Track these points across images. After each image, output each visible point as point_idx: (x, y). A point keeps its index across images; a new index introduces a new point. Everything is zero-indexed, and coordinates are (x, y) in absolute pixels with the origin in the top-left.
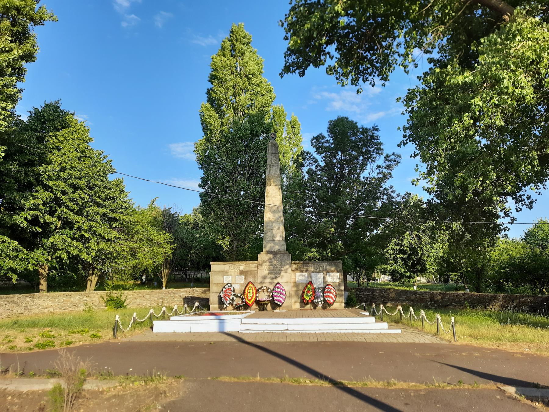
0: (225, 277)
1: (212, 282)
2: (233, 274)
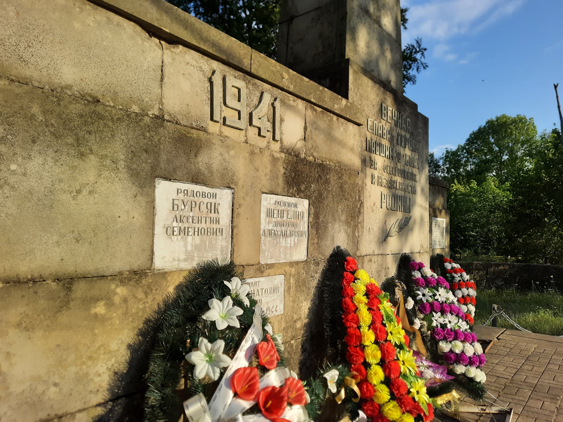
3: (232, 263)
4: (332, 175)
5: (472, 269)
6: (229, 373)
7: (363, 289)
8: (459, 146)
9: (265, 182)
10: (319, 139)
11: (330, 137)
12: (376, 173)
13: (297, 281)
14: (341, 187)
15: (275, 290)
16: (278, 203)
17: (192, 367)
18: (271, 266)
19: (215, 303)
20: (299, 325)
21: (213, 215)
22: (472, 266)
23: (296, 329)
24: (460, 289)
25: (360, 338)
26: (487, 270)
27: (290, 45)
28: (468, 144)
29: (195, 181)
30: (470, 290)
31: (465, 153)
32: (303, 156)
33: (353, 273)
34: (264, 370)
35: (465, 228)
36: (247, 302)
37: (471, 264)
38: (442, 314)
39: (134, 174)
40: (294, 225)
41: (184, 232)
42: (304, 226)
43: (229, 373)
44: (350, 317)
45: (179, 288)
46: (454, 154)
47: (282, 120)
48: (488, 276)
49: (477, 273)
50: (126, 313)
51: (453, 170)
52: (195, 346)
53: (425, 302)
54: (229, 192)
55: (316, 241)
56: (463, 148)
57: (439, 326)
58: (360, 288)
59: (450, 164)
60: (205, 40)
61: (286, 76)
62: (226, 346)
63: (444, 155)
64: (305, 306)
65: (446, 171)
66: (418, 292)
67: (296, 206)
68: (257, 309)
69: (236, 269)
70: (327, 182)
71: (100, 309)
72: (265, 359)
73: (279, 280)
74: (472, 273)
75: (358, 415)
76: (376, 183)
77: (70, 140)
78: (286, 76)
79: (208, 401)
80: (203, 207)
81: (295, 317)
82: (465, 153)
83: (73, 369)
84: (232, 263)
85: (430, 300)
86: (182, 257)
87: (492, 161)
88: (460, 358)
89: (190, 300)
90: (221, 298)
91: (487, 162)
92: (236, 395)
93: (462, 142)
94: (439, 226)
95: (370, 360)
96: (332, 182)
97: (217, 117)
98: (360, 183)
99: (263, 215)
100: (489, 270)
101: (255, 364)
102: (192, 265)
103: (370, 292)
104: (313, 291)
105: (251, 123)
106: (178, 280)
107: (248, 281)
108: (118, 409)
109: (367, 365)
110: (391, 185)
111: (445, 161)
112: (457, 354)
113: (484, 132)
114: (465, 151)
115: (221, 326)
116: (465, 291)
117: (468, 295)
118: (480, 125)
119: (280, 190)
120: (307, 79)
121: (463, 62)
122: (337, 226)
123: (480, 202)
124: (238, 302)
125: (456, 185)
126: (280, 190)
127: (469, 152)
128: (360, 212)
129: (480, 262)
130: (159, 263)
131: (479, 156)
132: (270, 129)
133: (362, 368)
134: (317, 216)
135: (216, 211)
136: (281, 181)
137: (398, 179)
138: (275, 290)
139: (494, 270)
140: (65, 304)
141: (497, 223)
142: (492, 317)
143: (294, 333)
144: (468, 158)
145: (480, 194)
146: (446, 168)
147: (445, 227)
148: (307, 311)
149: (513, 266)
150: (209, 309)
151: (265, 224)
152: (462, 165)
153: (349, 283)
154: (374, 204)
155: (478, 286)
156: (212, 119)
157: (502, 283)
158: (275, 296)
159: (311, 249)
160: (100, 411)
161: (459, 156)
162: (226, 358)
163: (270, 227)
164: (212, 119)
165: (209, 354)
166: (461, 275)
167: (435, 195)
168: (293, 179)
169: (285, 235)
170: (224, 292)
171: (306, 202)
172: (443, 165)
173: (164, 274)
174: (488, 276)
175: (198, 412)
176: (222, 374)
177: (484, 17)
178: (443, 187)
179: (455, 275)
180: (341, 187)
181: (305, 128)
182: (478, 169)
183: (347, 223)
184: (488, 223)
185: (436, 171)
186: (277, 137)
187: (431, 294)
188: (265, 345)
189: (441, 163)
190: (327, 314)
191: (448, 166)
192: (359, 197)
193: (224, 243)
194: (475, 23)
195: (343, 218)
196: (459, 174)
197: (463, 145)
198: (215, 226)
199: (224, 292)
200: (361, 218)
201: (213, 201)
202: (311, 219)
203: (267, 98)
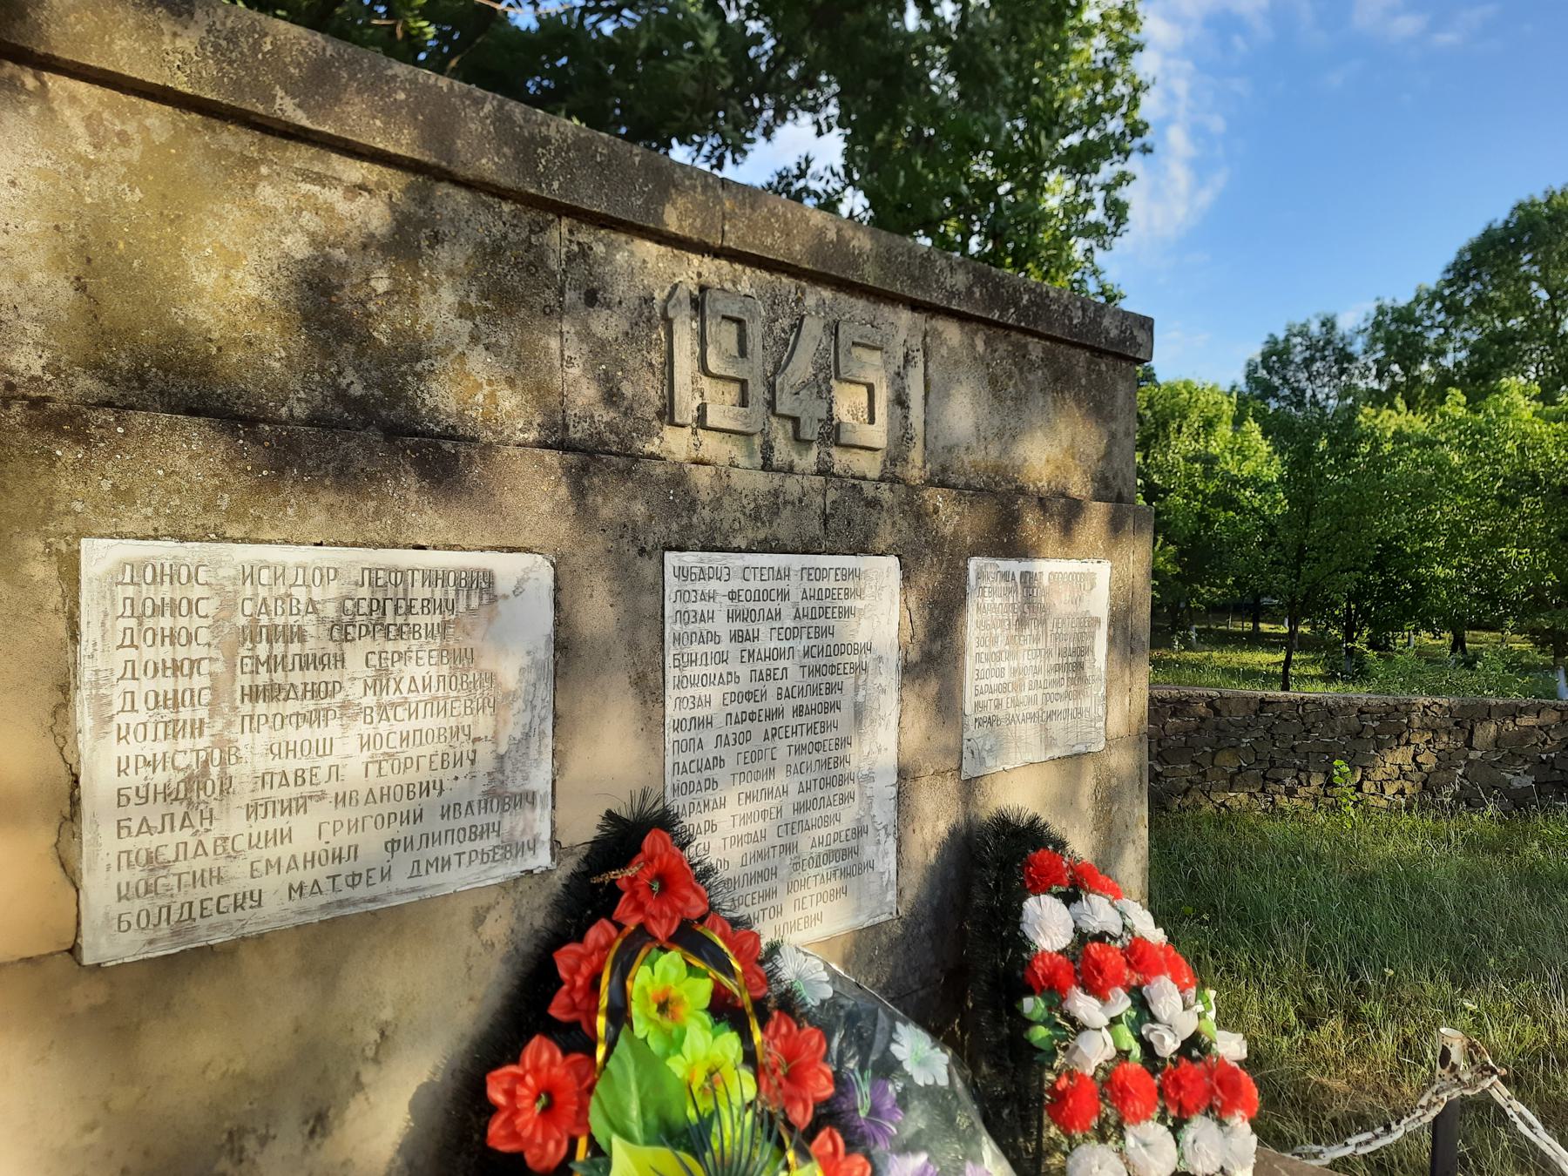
26: (1471, 733)
28: (1450, 283)
31: (1439, 312)
35: (1418, 555)
37: (1402, 708)
46: (1404, 316)
48: (1472, 755)
49: (1428, 742)
51: (1395, 368)
56: (1436, 296)
59: (1387, 349)
63: (1371, 321)
65: (1374, 372)
74: (1408, 743)
82: (1439, 312)
87: (1525, 337)
93: (1432, 275)
100: (1478, 732)
113: (1503, 241)
114: (1438, 305)
121: (1446, 38)
123: (1473, 465)
125: (1399, 413)
127: (1453, 309)
131: (1482, 323)
139: (1499, 730)
141: (1526, 540)
142: (1431, 1104)
144: (1446, 329)
145: (1475, 440)
146: (1376, 361)
152: (1427, 350)
157: (1529, 781)
161: (1418, 322)
167: (1019, 399)
172: (1366, 352)
174: (1472, 755)
178: (1097, 352)
179: (1084, 1005)
182: (1479, 361)
184: (1495, 540)
189: (1358, 347)
191: (1380, 355)
196: (1417, 380)
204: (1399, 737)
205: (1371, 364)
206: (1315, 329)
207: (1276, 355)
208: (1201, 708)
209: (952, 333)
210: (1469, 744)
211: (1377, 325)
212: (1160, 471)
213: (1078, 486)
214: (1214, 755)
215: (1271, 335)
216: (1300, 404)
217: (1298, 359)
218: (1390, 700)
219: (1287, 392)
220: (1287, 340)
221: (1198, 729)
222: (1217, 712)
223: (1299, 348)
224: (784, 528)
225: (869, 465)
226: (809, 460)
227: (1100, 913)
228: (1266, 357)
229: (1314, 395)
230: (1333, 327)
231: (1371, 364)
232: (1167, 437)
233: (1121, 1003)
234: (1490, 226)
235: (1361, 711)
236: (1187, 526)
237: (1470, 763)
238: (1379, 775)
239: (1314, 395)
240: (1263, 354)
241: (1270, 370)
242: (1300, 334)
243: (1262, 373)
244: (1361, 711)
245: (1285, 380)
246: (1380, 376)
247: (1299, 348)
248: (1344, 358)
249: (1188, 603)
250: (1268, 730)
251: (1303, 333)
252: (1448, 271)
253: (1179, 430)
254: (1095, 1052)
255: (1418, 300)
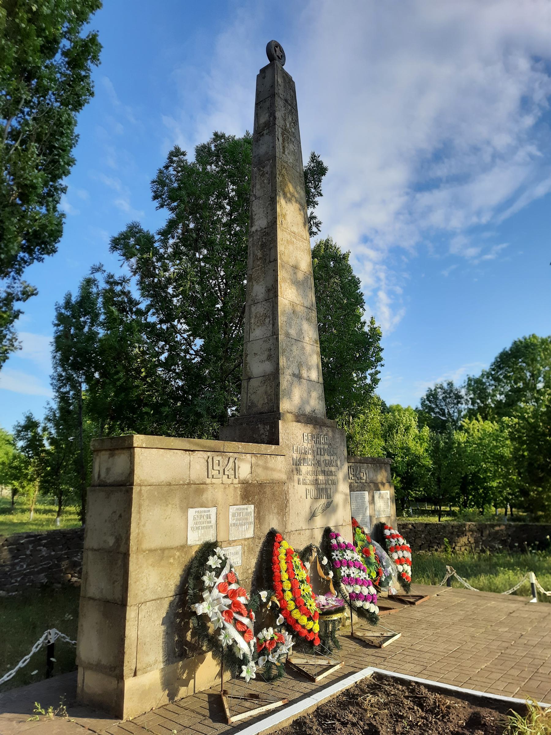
0: (192, 512)
1: (139, 542)
2: (219, 495)
3: (217, 541)
4: (267, 488)
5: (465, 530)
6: (217, 584)
7: (284, 551)
8: (483, 371)
9: (231, 500)
10: (259, 471)
11: (266, 468)
12: (301, 478)
13: (249, 548)
14: (273, 494)
15: (237, 553)
16: (237, 509)
17: (204, 582)
18: (235, 541)
19: (211, 558)
20: (250, 571)
21: (208, 520)
22: (465, 527)
23: (248, 574)
24: (396, 552)
25: (280, 577)
27: (249, 395)
29: (202, 507)
30: (405, 552)
32: (250, 482)
33: (279, 543)
34: (230, 584)
35: (484, 478)
36: (223, 558)
38: (348, 568)
39: (181, 508)
40: (247, 519)
41: (198, 528)
42: (251, 519)
43: (217, 584)
44: (275, 566)
45: (196, 552)
46: (478, 381)
47: (239, 467)
48: (484, 538)
50: (179, 562)
51: (478, 401)
52: (204, 574)
53: (337, 560)
54: (215, 508)
55: (259, 526)
56: (488, 375)
57: (346, 576)
58: (282, 552)
60: (205, 447)
61: (240, 447)
62: (216, 574)
63: (466, 383)
64: (253, 562)
65: (470, 402)
66: (333, 553)
67: (247, 509)
68: (228, 561)
69: (219, 544)
70: (265, 493)
71: (172, 560)
72: (230, 579)
73: (239, 548)
74: (466, 535)
75: (279, 616)
76: (302, 484)
77: (164, 501)
78: (240, 447)
79: (210, 593)
80: (205, 517)
81: (248, 567)
83: (164, 582)
84: (217, 541)
85: (341, 558)
86: (197, 539)
88: (359, 596)
89: (201, 557)
90: (213, 556)
91: (519, 390)
92: (220, 592)
94: (383, 498)
95: (285, 588)
96: (268, 493)
97: (210, 476)
98: (286, 489)
99: (230, 516)
101: (227, 580)
102: (201, 542)
103: (288, 553)
104: (257, 553)
105: (224, 474)
106: (196, 549)
107: (224, 549)
108: (177, 599)
109: (284, 591)
110: (316, 482)
111: (469, 390)
112: (357, 594)
114: (491, 378)
115: (214, 567)
116: (400, 553)
117: (403, 557)
118: (504, 347)
119: (238, 503)
120: (251, 444)
121: (488, 257)
122: (271, 516)
124: (219, 558)
126: (238, 503)
128: (286, 506)
129: (474, 523)
130: (189, 543)
132: (233, 474)
133: (281, 592)
134: (259, 513)
135: (210, 518)
136: (239, 498)
137: (321, 478)
138: (237, 553)
140: (162, 559)
143: (247, 576)
144: (496, 386)
146: (471, 398)
147: (389, 497)
148: (254, 564)
149: (510, 525)
150: (208, 560)
151: (231, 521)
153: (277, 549)
154: (301, 497)
155: (413, 549)
156: (208, 477)
158: (237, 556)
159: (256, 531)
160: (172, 599)
162: (215, 578)
163: (234, 522)
164: (208, 477)
165: (209, 577)
166: (398, 540)
168: (245, 496)
169: (241, 525)
170: (214, 554)
171: (253, 506)
172: (466, 395)
173: (191, 547)
174: (484, 538)
175: (207, 596)
176: (214, 585)
177: (509, 202)
179: (392, 540)
180: (273, 494)
181: (252, 467)
183: (278, 513)
185: (458, 402)
186: (237, 477)
187: (341, 554)
188: (230, 574)
189: (463, 392)
190: (264, 565)
191: (472, 396)
192: (286, 497)
193: (213, 532)
194: (500, 208)
195: (276, 511)
196: (487, 406)
197: (488, 370)
198: (210, 525)
199: (214, 554)
200: (287, 509)
201: (208, 513)
202: (255, 515)
203: (232, 460)
204: (463, 534)
205: (469, 399)
206: (445, 386)
207: (432, 396)
208: (410, 526)
209: (370, 465)
210: (482, 535)
211: (469, 385)
212: (391, 448)
213: (384, 481)
214: (415, 540)
215: (429, 388)
216: (444, 415)
217: (441, 398)
218: (460, 523)
219: (437, 410)
220: (435, 390)
221: (410, 533)
222: (415, 528)
223: (440, 393)
224: (358, 489)
225: (364, 481)
226: (359, 482)
227: (393, 531)
228: (428, 397)
229: (449, 412)
230: (452, 385)
231: (469, 399)
232: (393, 435)
233: (396, 539)
234: (504, 350)
235: (452, 527)
236: (402, 469)
237: (483, 541)
238: (459, 545)
239: (449, 412)
240: (427, 395)
241: (430, 401)
242: (440, 388)
243: (427, 402)
244: (452, 527)
245: (437, 405)
246: (473, 404)
247: (440, 393)
248: (458, 397)
249: (408, 498)
250: (429, 532)
251: (441, 388)
252: (492, 365)
253: (397, 433)
254: (393, 544)
255: (483, 375)
